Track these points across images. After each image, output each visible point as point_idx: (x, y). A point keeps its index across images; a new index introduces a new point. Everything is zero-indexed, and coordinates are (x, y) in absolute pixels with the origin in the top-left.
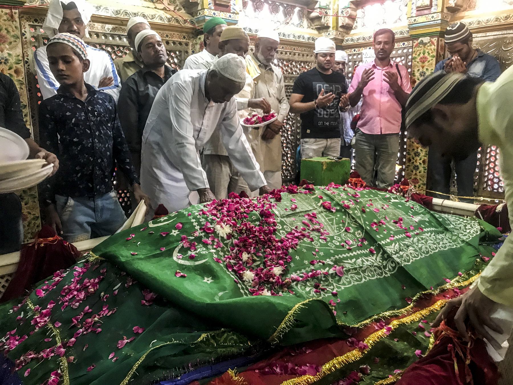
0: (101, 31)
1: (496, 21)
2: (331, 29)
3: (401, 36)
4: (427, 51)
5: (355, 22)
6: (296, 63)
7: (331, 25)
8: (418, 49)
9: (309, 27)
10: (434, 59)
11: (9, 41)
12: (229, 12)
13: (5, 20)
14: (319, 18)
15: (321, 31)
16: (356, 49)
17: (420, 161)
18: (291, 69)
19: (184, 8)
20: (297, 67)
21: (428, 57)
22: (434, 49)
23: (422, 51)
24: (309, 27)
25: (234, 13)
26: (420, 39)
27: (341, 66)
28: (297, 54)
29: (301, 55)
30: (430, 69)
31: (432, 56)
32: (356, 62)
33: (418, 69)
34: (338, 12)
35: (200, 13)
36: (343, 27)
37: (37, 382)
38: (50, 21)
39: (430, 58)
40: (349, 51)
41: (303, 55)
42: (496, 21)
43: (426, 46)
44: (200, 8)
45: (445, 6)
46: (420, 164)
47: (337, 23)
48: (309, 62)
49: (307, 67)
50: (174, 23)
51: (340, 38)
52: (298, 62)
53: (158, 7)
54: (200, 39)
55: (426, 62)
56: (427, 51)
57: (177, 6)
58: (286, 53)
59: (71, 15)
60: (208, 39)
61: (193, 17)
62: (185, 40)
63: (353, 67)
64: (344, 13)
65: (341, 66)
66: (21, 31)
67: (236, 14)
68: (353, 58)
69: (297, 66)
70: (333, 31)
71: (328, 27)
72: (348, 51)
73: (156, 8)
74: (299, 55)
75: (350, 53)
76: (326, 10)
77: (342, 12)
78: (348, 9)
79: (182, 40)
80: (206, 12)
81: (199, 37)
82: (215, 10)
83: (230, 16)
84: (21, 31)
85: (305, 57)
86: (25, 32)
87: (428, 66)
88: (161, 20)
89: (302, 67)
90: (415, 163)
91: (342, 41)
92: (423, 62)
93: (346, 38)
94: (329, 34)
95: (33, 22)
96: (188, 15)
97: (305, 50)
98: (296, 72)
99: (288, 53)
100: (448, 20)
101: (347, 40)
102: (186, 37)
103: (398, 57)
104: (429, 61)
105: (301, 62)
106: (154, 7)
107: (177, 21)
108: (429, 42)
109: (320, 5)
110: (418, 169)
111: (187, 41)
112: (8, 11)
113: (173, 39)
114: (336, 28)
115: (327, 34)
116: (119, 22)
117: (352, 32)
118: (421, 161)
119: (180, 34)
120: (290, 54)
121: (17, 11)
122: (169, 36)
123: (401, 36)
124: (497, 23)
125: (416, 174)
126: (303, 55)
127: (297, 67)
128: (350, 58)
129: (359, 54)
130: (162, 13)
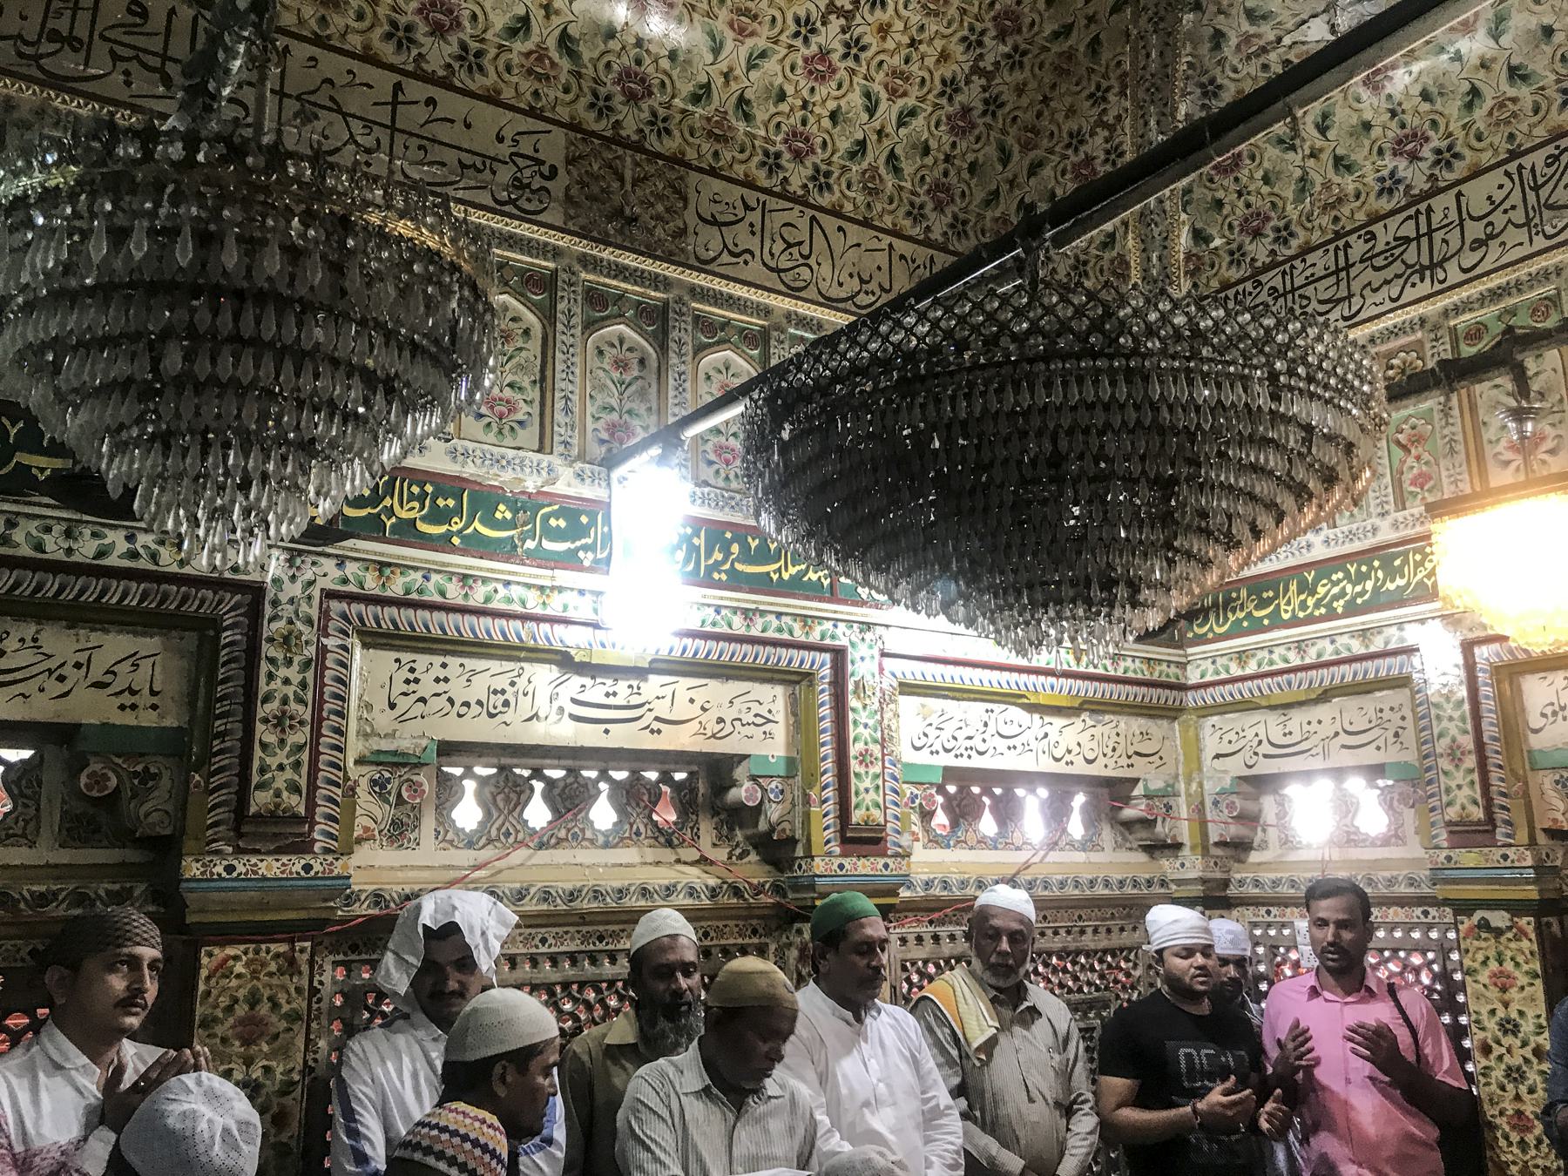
0: (524, 951)
2: (1186, 851)
3: (1412, 890)
4: (1509, 954)
6: (1087, 956)
8: (1476, 943)
9: (1117, 846)
10: (1539, 983)
11: (273, 1030)
12: (884, 855)
13: (271, 974)
14: (1148, 823)
15: (1157, 853)
16: (1274, 910)
17: (1522, 1052)
18: (1076, 979)
19: (755, 847)
20: (1092, 969)
21: (1517, 974)
22: (1532, 953)
23: (1492, 953)
24: (1117, 846)
25: (896, 855)
26: (1478, 915)
27: (1232, 971)
28: (1089, 930)
29: (1102, 930)
30: (1530, 1013)
31: (1527, 973)
32: (1277, 948)
33: (1490, 1007)
34: (1202, 803)
35: (800, 867)
36: (1221, 844)
38: (388, 970)
41: (1109, 931)
43: (1503, 939)
44: (799, 852)
45: (1538, 826)
46: (1527, 1061)
47: (1204, 834)
48: (1130, 950)
49: (1123, 964)
50: (728, 900)
51: (1218, 875)
52: (1096, 952)
53: (683, 858)
54: (799, 932)
56: (1509, 954)
57: (737, 845)
58: (1056, 933)
59: (445, 954)
60: (824, 958)
61: (781, 871)
62: (755, 940)
63: (1272, 961)
64: (1223, 806)
65: (1232, 971)
66: (311, 981)
67: (903, 857)
68: (1266, 934)
69: (1092, 966)
71: (1178, 846)
73: (678, 861)
74: (1096, 931)
76: (1165, 800)
77: (1216, 803)
78: (1234, 798)
79: (747, 941)
80: (819, 866)
81: (797, 925)
82: (844, 855)
83: (886, 866)
84: (311, 981)
85: (1115, 935)
86: (321, 983)
88: (691, 895)
89: (1110, 966)
91: (1226, 883)
92: (1504, 990)
93: (1238, 876)
94: (1183, 865)
95: (345, 954)
96: (768, 868)
97: (1113, 917)
98: (1089, 984)
99: (1062, 932)
100: (1558, 863)
101: (1241, 883)
102: (761, 931)
104: (1522, 988)
105: (1105, 952)
106: (674, 858)
107: (737, 892)
108: (1510, 928)
109: (1146, 787)
111: (763, 940)
112: (283, 948)
113: (723, 942)
114: (1204, 848)
116: (577, 919)
117: (1254, 857)
118: (1528, 1052)
119: (741, 923)
120: (1069, 932)
121: (308, 944)
122: (712, 934)
123: (1412, 890)
125: (1518, 1098)
126: (1109, 931)
127: (1092, 969)
128: (1258, 932)
129: (1284, 925)
130: (694, 876)
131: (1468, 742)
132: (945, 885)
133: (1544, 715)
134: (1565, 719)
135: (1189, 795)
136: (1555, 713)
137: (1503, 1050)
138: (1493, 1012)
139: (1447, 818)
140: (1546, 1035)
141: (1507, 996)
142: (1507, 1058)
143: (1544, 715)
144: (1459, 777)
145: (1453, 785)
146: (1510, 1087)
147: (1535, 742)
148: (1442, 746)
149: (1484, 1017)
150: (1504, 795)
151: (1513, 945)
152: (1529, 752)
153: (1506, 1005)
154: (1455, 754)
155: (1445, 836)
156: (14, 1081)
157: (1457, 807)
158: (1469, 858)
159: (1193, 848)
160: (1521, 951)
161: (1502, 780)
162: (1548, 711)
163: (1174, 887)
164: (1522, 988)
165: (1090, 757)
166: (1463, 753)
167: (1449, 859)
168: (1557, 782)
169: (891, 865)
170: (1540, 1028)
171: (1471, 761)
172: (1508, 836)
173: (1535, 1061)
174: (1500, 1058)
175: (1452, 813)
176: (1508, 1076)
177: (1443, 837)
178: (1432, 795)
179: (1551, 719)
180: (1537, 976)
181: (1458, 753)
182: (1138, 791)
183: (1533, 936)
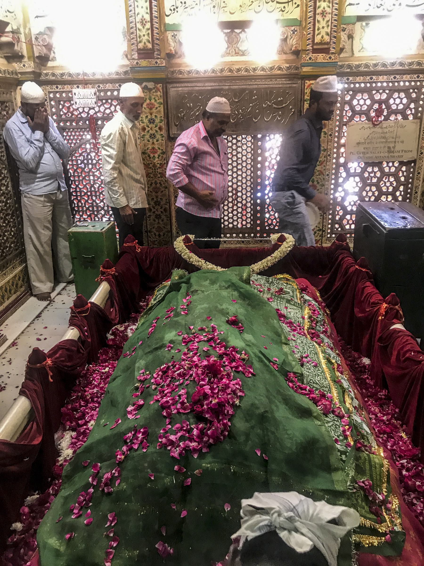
1: (213, 72)
2: (26, 59)
4: (153, 97)
5: (52, 52)
7: (25, 53)
10: (162, 106)
14: (10, 45)
15: (11, 60)
16: (60, 87)
17: (155, 129)
21: (155, 104)
30: (159, 116)
33: (146, 115)
34: (31, 38)
37: (9, 347)
39: (157, 105)
40: (48, 88)
42: (213, 72)
43: (152, 92)
55: (154, 109)
56: (153, 97)
70: (29, 62)
72: (47, 88)
75: (51, 90)
77: (36, 39)
87: (157, 112)
90: (156, 212)
92: (151, 109)
93: (45, 72)
94: (24, 66)
101: (47, 75)
103: (115, 99)
104: (157, 108)
108: (154, 88)
110: (160, 217)
114: (32, 57)
115: (22, 65)
117: (50, 64)
118: (157, 129)
123: (118, 77)
124: (213, 75)
125: (153, 143)
131: (147, 17)
132: (231, 70)
133: (171, 10)
134: (177, 12)
135: (25, 34)
136: (174, 10)
137: (149, 129)
138: (147, 117)
139: (139, 47)
140: (163, 123)
141: (152, 111)
142: (150, 131)
143: (171, 10)
144: (144, 32)
145: (142, 35)
146: (151, 140)
147: (168, 20)
148: (138, 19)
149: (144, 119)
150: (157, 39)
151: (155, 94)
152: (165, 24)
153: (151, 114)
154: (143, 22)
155: (137, 55)
156: (153, 302)
157: (143, 44)
158: (144, 63)
159: (29, 58)
160: (157, 96)
161: (157, 34)
162: (172, 8)
163: (20, 76)
164: (157, 108)
165: (389, 9)
166: (146, 22)
167: (137, 63)
168: (172, 36)
169: (333, 58)
170: (161, 121)
171: (148, 25)
172: (158, 55)
173: (159, 131)
174: (148, 131)
175: (141, 46)
176: (150, 137)
177: (136, 56)
178: (133, 38)
179: (173, 11)
180: (162, 104)
181: (144, 22)
182: (8, 29)
183: (161, 91)
